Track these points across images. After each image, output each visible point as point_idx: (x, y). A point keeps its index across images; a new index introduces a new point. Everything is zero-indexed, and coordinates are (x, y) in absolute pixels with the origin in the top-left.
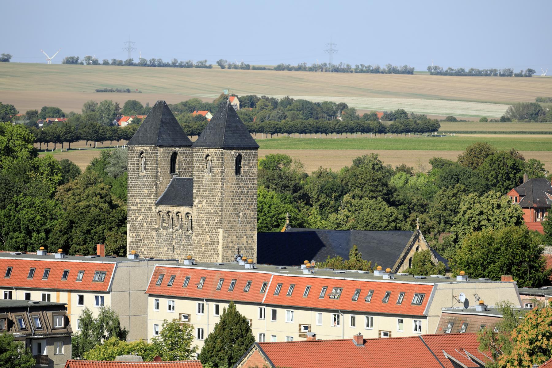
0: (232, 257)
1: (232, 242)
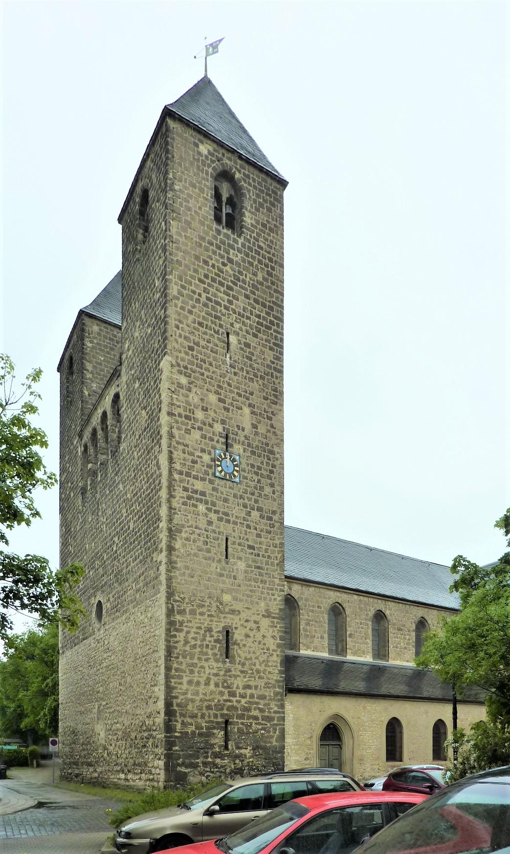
0: (203, 451)
1: (205, 409)
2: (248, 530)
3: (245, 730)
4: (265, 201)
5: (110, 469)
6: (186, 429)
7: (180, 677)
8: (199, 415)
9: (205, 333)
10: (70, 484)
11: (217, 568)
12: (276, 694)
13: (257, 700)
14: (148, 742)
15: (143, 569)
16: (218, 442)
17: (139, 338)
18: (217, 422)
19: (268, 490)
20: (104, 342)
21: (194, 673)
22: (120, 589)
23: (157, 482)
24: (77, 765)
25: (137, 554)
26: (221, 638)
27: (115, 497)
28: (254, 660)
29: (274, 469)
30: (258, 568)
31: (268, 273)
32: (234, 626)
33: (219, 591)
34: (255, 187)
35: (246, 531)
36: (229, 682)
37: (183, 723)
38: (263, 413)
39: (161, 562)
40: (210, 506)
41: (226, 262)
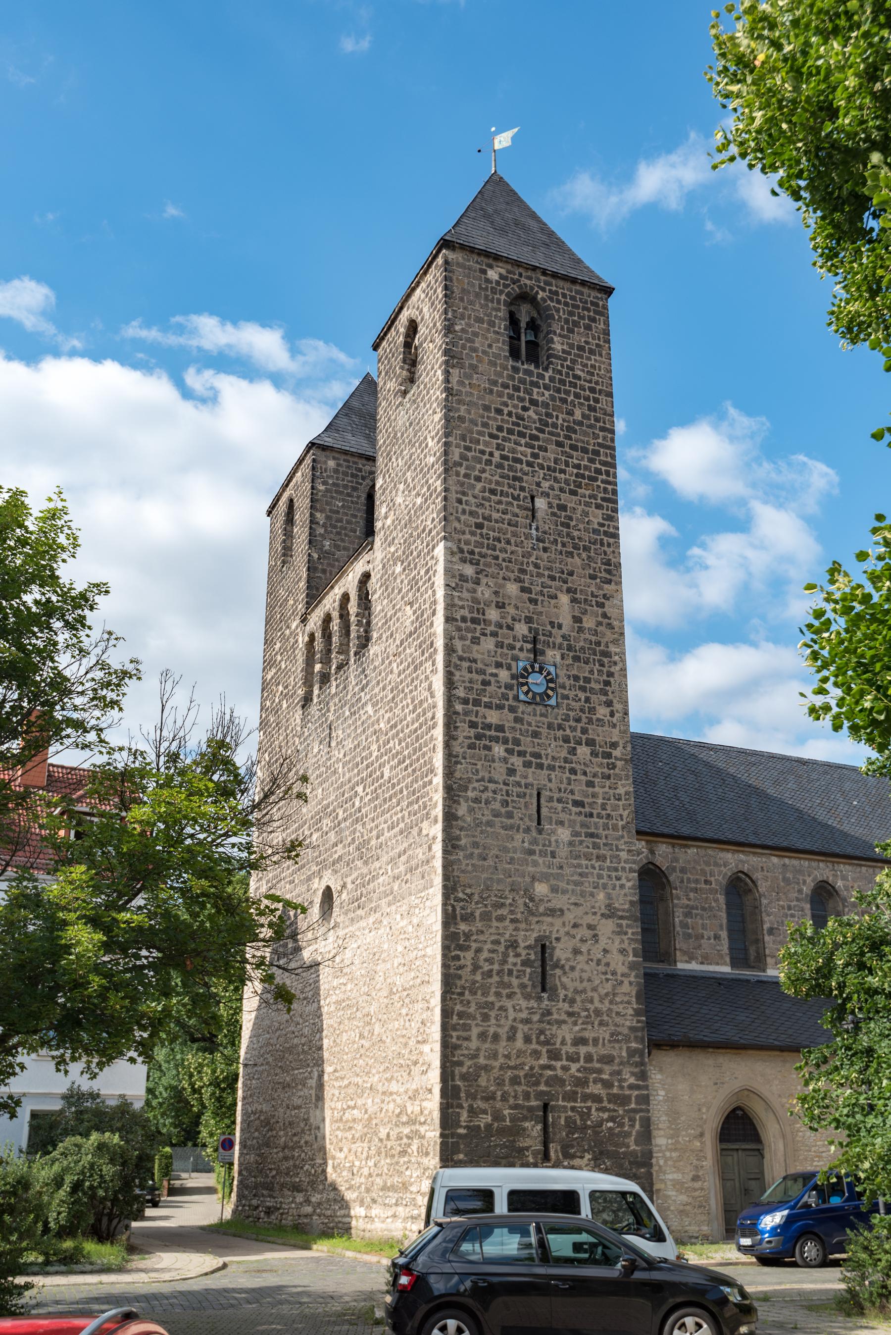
0: (499, 665)
1: (500, 606)
2: (573, 777)
3: (578, 1122)
4: (580, 317)
5: (352, 680)
6: (473, 638)
7: (466, 1028)
8: (493, 614)
9: (500, 502)
10: (281, 688)
11: (523, 842)
12: (632, 1053)
13: (598, 1065)
14: (409, 1145)
15: (405, 845)
16: (521, 649)
17: (403, 507)
18: (520, 621)
19: (602, 712)
20: (343, 480)
21: (489, 1020)
22: (365, 870)
23: (429, 715)
24: (272, 1189)
25: (395, 818)
26: (533, 957)
27: (359, 723)
28: (590, 994)
29: (612, 680)
30: (592, 835)
31: (592, 409)
32: (554, 936)
33: (528, 879)
34: (566, 304)
35: (569, 779)
36: (548, 1033)
37: (472, 1112)
38: (590, 598)
39: (434, 838)
40: (510, 746)
41: (527, 405)
